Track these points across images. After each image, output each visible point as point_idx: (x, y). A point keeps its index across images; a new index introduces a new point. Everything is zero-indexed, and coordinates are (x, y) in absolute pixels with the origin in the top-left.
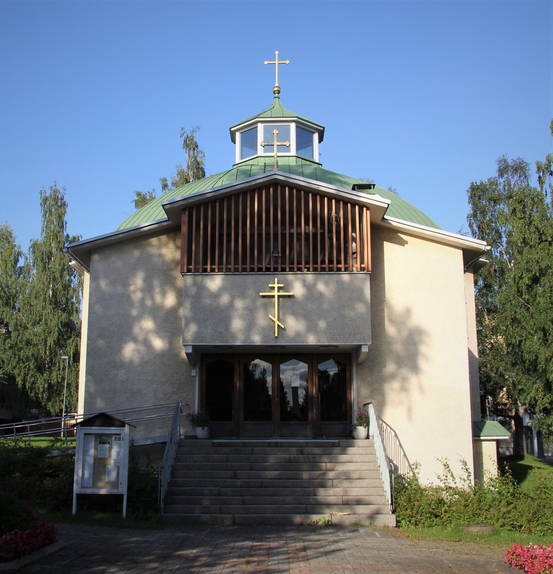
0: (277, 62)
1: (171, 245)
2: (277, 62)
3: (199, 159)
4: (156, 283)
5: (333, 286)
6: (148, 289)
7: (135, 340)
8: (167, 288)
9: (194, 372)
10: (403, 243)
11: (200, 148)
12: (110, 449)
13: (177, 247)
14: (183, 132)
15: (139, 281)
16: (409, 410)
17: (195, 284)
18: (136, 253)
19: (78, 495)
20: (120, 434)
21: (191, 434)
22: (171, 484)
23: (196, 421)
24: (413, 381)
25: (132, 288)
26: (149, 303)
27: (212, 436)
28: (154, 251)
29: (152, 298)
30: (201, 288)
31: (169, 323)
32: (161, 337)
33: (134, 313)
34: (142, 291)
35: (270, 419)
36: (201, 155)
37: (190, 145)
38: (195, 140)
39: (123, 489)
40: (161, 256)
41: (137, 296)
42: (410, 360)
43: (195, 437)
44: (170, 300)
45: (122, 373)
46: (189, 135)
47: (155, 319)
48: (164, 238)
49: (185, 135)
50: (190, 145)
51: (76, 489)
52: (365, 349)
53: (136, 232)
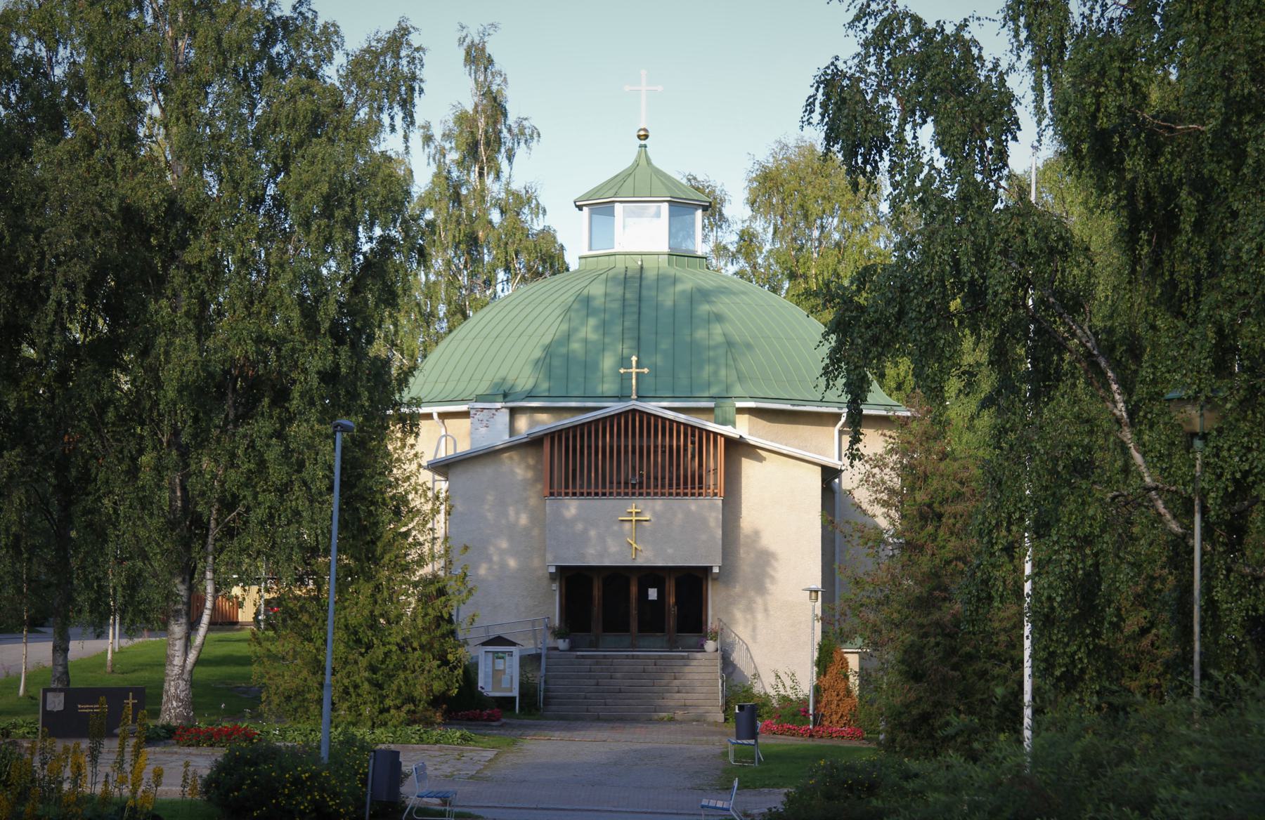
0: (634, 370)
2: (634, 370)
3: (494, 88)
9: (555, 586)
10: (760, 459)
11: (497, 67)
14: (464, 34)
16: (754, 629)
21: (553, 645)
22: (546, 690)
23: (558, 634)
27: (572, 648)
35: (628, 631)
36: (498, 80)
39: (515, 693)
42: (759, 583)
43: (556, 649)
49: (468, 40)
52: (716, 570)
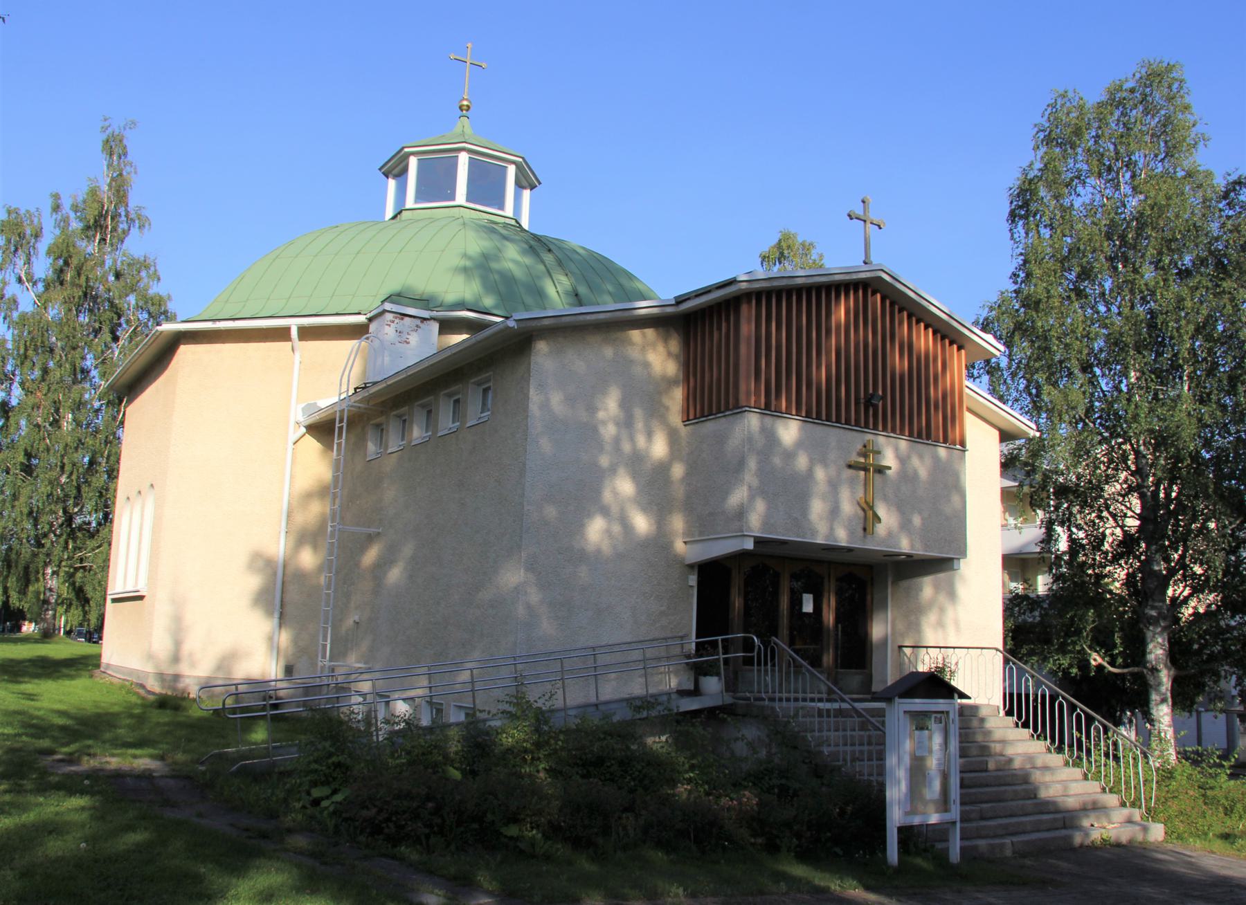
1: (661, 348)
4: (638, 413)
5: (928, 461)
6: (627, 423)
7: (605, 511)
8: (655, 424)
11: (130, 158)
12: (930, 738)
13: (669, 354)
15: (611, 405)
17: (763, 429)
18: (608, 352)
19: (900, 829)
20: (948, 712)
24: (950, 613)
25: (601, 415)
26: (626, 447)
28: (634, 353)
29: (632, 439)
30: (771, 439)
31: (654, 486)
32: (645, 509)
33: (604, 461)
34: (617, 424)
36: (128, 169)
37: (114, 147)
38: (125, 142)
40: (647, 365)
41: (609, 431)
44: (659, 448)
45: (583, 572)
46: (117, 132)
47: (635, 476)
48: (650, 332)
49: (110, 131)
50: (114, 147)
51: (896, 816)
53: (626, 314)
